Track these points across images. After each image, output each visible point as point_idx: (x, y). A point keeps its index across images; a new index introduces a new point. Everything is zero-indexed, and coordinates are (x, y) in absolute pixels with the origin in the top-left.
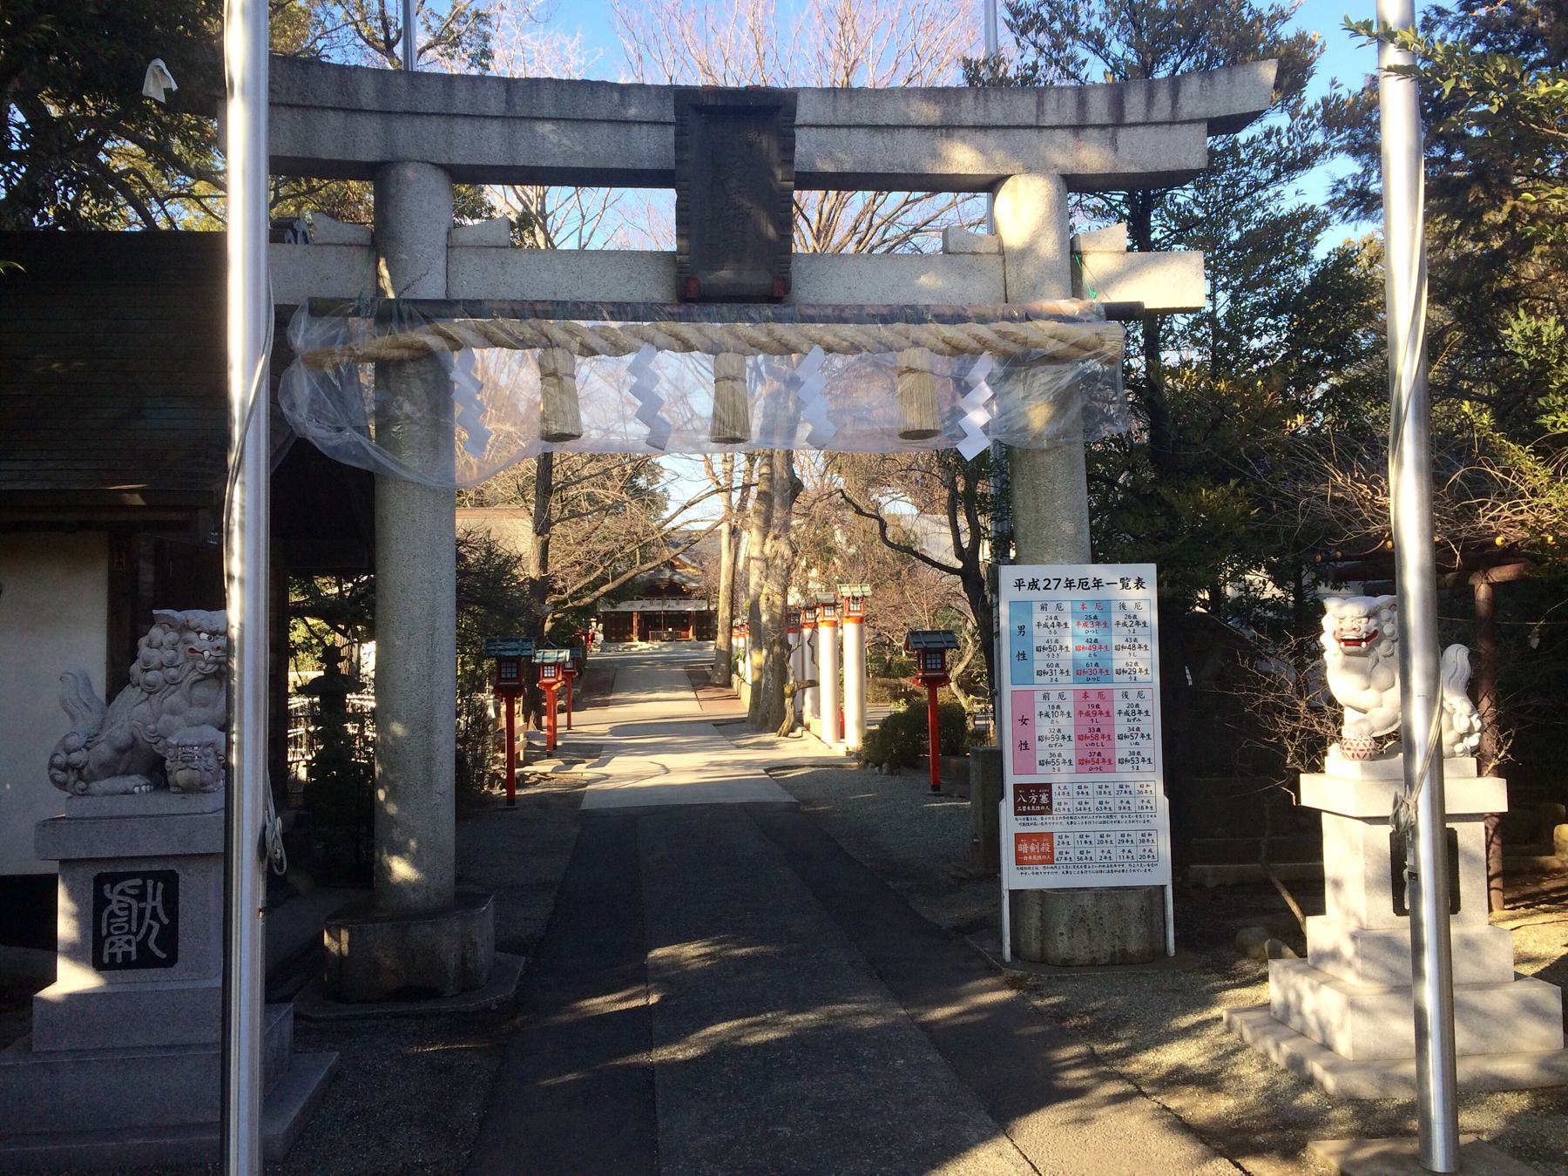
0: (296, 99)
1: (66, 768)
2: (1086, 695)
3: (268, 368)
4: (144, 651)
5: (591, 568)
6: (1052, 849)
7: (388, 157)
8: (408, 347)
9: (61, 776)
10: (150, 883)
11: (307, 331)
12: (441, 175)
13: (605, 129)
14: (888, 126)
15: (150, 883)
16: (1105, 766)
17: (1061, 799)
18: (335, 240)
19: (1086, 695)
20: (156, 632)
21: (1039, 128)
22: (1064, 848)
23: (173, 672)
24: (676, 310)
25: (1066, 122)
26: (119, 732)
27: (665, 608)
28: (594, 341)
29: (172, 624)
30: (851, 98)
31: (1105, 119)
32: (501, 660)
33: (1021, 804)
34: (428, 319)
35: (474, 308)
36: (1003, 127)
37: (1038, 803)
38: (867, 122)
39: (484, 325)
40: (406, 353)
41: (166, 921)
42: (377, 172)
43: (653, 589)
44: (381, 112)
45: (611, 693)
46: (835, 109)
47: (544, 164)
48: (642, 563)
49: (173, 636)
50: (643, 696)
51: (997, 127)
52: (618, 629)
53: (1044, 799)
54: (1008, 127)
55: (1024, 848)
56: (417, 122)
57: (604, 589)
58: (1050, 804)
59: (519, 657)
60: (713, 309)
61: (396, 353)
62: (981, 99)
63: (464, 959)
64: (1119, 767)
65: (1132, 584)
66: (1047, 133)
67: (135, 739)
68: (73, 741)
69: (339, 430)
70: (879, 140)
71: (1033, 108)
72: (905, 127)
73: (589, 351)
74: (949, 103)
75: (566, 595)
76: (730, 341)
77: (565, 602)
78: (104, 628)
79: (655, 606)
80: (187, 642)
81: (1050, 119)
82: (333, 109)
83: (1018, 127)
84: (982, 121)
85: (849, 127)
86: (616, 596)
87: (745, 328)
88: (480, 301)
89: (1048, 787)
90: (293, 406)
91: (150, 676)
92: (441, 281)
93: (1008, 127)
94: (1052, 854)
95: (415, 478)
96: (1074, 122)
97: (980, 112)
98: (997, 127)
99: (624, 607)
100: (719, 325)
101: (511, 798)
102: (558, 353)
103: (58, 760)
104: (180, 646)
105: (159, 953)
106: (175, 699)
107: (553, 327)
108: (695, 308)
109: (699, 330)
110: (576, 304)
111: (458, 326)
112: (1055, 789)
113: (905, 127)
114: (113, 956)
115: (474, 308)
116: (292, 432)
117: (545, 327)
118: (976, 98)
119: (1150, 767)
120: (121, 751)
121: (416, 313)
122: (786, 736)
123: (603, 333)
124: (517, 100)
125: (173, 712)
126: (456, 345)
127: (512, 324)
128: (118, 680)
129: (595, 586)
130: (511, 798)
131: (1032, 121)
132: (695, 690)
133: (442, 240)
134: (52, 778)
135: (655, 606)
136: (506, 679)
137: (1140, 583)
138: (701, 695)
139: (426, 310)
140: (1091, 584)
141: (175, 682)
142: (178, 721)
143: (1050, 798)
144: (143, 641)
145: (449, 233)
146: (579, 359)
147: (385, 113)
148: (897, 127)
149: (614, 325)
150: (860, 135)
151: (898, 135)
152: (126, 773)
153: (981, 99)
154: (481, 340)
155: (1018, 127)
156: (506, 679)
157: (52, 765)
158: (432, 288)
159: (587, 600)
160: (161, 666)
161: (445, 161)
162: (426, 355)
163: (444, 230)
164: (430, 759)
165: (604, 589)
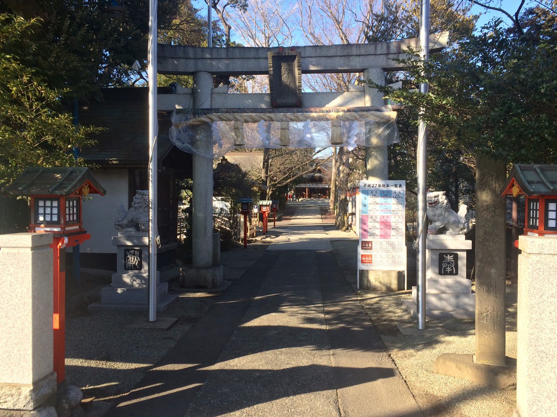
0: (173, 56)
1: (118, 225)
2: (383, 217)
3: (156, 145)
4: (135, 200)
5: (285, 173)
6: (372, 259)
7: (196, 70)
8: (200, 121)
9: (117, 227)
10: (136, 252)
11: (175, 118)
12: (210, 75)
13: (253, 60)
14: (331, 56)
15: (136, 252)
16: (388, 237)
17: (375, 245)
18: (183, 93)
19: (383, 217)
20: (137, 195)
21: (376, 55)
22: (375, 245)
23: (140, 204)
24: (270, 110)
25: (383, 53)
26: (129, 218)
27: (317, 187)
28: (249, 119)
29: (140, 194)
30: (320, 49)
31: (395, 52)
32: (242, 204)
33: (364, 246)
34: (205, 114)
35: (217, 110)
36: (364, 55)
37: (368, 246)
38: (325, 55)
39: (219, 115)
40: (200, 123)
41: (139, 260)
42: (194, 74)
43: (313, 180)
44: (194, 59)
45: (292, 215)
46: (316, 52)
47: (236, 71)
48: (302, 172)
49: (140, 196)
50: (302, 217)
51: (363, 55)
52: (299, 193)
53: (370, 245)
54: (366, 55)
55: (364, 259)
56: (204, 60)
57: (289, 181)
58: (372, 247)
59: (248, 203)
60: (280, 109)
61: (197, 123)
62: (358, 47)
63: (213, 279)
64: (392, 237)
65: (398, 186)
66: (378, 56)
67: (133, 219)
68: (120, 219)
69: (183, 143)
70: (329, 60)
71: (374, 49)
72: (336, 56)
73: (247, 122)
74: (349, 49)
75: (276, 182)
76: (284, 118)
77: (276, 184)
78: (128, 193)
79: (314, 186)
80: (144, 198)
81: (379, 52)
82: (183, 58)
83: (369, 55)
84: (358, 54)
85: (320, 57)
86: (296, 182)
87: (289, 114)
88: (218, 109)
89: (371, 242)
90: (172, 137)
91: (136, 205)
92: (209, 103)
93: (366, 55)
94: (372, 261)
95: (203, 155)
96: (386, 53)
97: (358, 51)
98: (363, 55)
99: (303, 186)
100: (282, 114)
101: (245, 246)
102: (239, 122)
103: (117, 223)
104: (142, 199)
105: (138, 267)
106: (141, 211)
107: (237, 115)
108: (275, 109)
109: (276, 116)
110: (243, 109)
111: (214, 116)
112: (373, 257)
113: (336, 56)
114: (128, 267)
115: (217, 110)
116: (172, 144)
117: (235, 116)
118: (357, 47)
119: (402, 238)
120: (130, 222)
121: (202, 112)
122: (345, 231)
123: (250, 117)
124: (229, 54)
125: (140, 214)
126: (213, 121)
127: (228, 115)
128: (130, 206)
129: (286, 179)
130: (245, 246)
131: (373, 53)
132: (322, 215)
133: (210, 92)
134: (115, 227)
135: (314, 186)
136: (244, 209)
137: (400, 186)
138: (323, 216)
139: (205, 111)
140: (386, 186)
141: (141, 207)
142: (141, 215)
143: (372, 245)
144: (134, 197)
145: (211, 90)
146: (245, 124)
147: (195, 59)
148: (334, 56)
149: (253, 114)
150: (324, 59)
151: (334, 59)
152: (131, 227)
153: (358, 47)
154: (218, 119)
155: (369, 55)
156: (244, 209)
157: (115, 225)
158: (207, 105)
159: (284, 184)
160: (138, 203)
161: (211, 71)
162: (205, 123)
163: (210, 89)
164: (206, 228)
165: (289, 181)
